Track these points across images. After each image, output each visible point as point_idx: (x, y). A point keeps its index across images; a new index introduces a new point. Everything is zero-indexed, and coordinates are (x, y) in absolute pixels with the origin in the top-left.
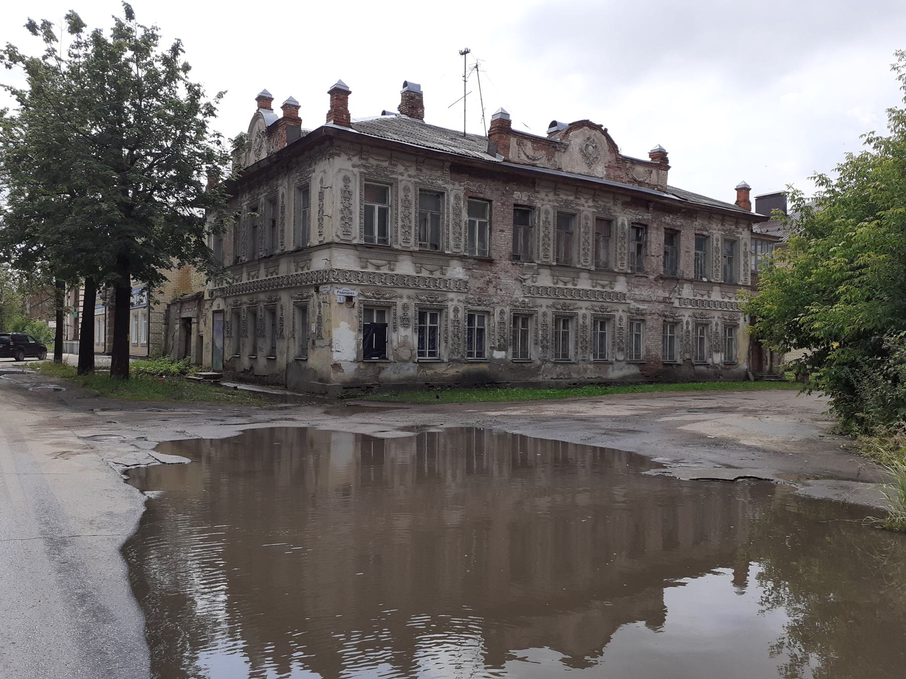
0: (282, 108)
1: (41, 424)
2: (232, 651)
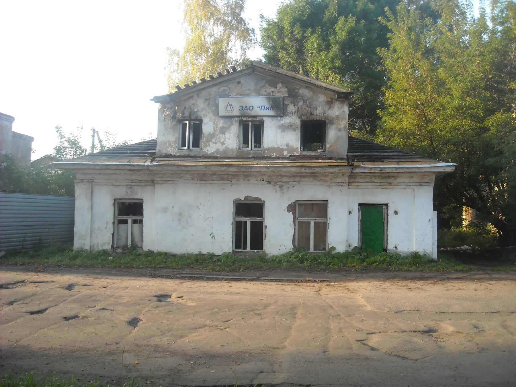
0: (31, 139)
1: (216, 384)
2: (430, 252)
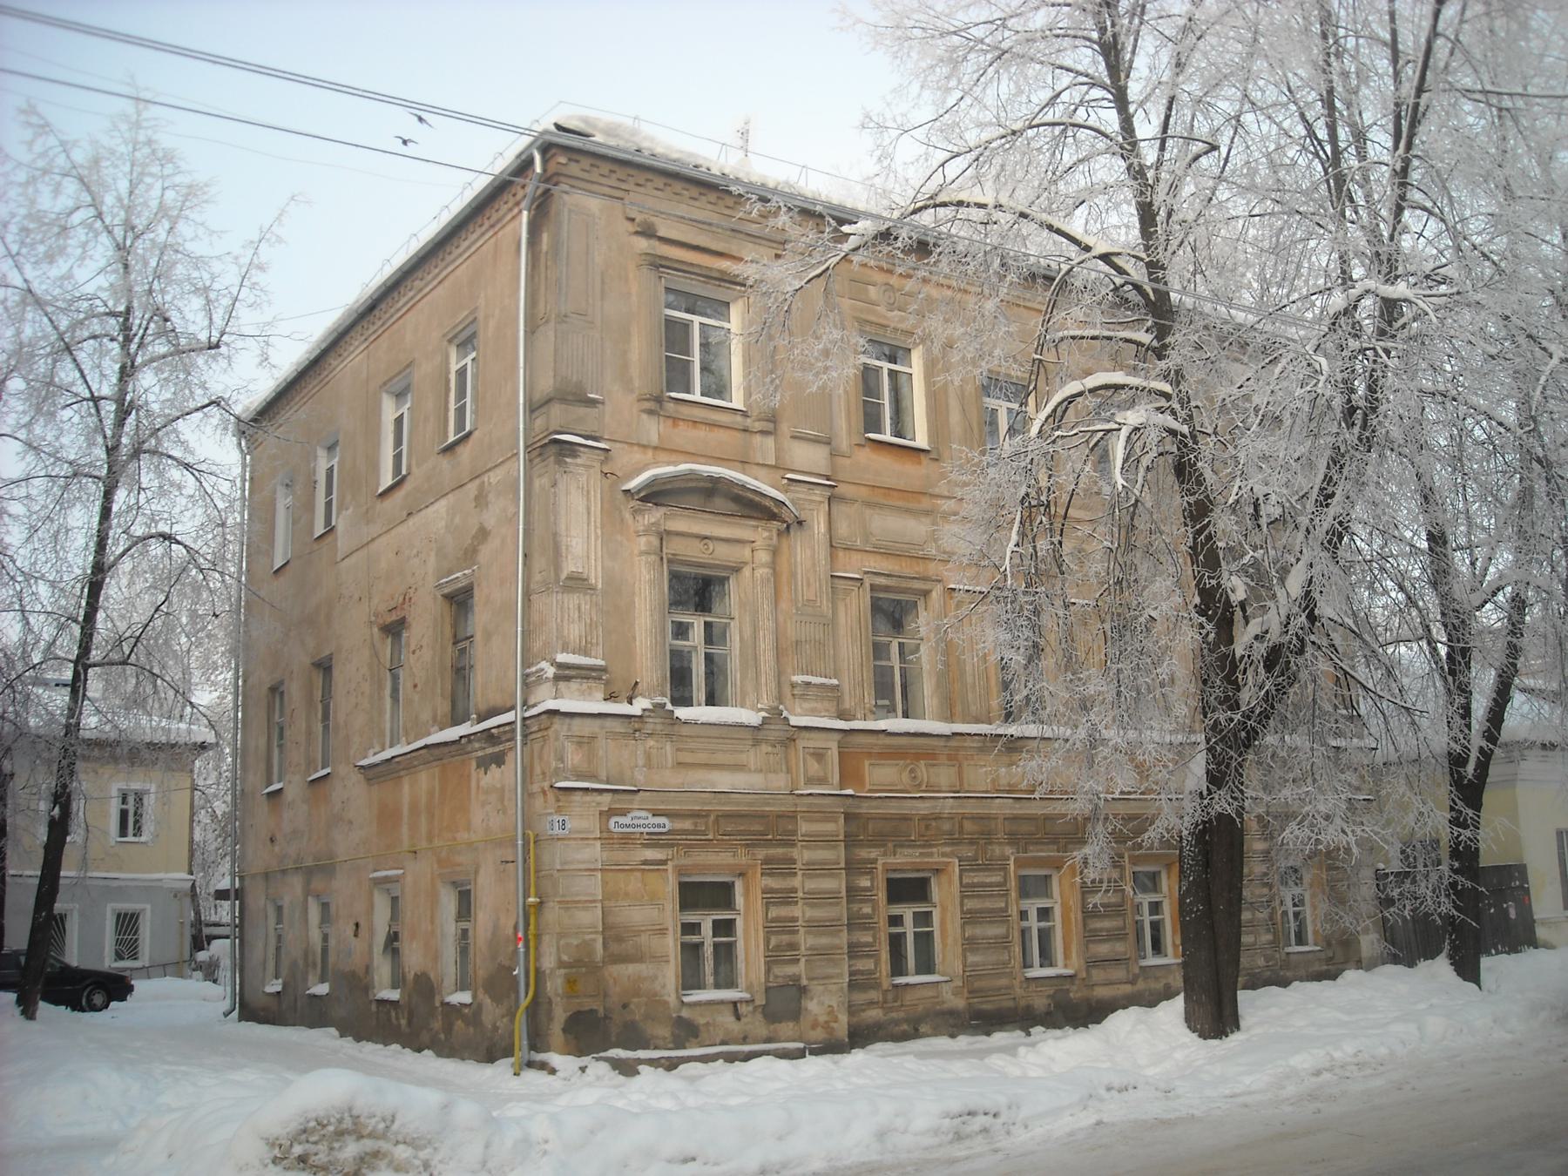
2: (244, 411)
